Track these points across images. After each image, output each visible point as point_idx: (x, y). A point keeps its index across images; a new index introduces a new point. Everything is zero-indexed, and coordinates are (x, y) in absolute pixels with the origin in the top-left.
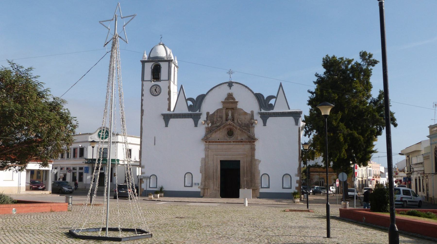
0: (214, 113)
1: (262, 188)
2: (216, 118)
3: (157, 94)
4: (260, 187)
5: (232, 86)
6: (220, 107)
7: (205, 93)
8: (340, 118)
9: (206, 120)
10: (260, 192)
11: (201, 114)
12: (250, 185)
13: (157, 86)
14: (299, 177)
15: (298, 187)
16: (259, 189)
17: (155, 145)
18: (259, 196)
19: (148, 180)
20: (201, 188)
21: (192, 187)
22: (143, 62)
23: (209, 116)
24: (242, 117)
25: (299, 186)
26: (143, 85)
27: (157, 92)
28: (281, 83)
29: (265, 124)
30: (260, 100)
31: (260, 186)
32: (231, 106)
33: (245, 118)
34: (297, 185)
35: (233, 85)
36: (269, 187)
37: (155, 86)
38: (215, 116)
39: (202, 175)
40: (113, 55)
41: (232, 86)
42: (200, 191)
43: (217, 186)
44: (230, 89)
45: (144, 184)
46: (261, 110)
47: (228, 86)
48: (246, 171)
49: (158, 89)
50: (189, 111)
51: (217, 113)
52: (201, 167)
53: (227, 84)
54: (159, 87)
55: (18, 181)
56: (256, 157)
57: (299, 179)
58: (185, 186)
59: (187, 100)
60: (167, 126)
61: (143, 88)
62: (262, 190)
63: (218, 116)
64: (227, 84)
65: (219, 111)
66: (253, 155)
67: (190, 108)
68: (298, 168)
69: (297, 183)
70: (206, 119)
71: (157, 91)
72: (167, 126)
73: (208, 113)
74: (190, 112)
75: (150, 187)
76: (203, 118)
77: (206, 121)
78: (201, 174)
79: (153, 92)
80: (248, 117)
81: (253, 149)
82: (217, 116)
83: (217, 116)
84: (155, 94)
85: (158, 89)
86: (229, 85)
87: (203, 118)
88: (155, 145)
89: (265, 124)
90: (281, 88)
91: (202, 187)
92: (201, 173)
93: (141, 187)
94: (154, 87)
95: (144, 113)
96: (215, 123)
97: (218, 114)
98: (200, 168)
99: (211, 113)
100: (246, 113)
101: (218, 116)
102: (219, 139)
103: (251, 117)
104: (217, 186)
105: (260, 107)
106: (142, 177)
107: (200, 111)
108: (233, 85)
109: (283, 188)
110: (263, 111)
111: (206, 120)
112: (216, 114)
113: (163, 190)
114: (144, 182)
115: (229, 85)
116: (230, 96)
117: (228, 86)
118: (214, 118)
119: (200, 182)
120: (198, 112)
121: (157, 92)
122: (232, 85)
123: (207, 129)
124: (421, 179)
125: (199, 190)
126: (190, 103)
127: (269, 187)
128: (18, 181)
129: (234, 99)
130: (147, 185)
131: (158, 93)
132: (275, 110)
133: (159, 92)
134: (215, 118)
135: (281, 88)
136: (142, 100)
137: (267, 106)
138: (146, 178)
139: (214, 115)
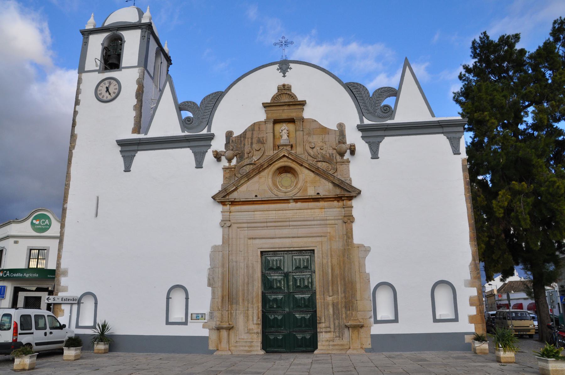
0: (245, 133)
1: (377, 322)
2: (250, 144)
3: (109, 98)
4: (372, 320)
5: (289, 70)
6: (261, 116)
7: (223, 90)
8: (543, 145)
9: (225, 150)
10: (371, 335)
11: (211, 137)
12: (344, 316)
13: (112, 81)
14: (475, 288)
15: (475, 315)
16: (369, 328)
17: (97, 215)
18: (370, 347)
19: (75, 307)
20: (211, 328)
21: (187, 325)
22: (86, 33)
23: (231, 142)
24: (316, 140)
25: (477, 314)
26: (80, 82)
27: (110, 94)
28: (406, 58)
29: (375, 155)
30: (358, 98)
31: (370, 317)
32: (286, 113)
33: (325, 142)
34: (473, 311)
35: (291, 68)
36: (396, 320)
37: (106, 82)
38: (246, 139)
39: (213, 293)
40: (321, 353)
41: (289, 70)
42: (208, 336)
43: (255, 322)
44: (284, 76)
45: (63, 317)
46: (362, 120)
47: (280, 71)
48: (330, 278)
49: (115, 89)
50: (183, 131)
51: (252, 134)
52: (212, 270)
53: (277, 66)
54: (115, 83)
55: (299, 247)
56: (357, 239)
57: (477, 295)
58: (168, 323)
59: (180, 108)
60: (127, 169)
61: (81, 88)
62: (376, 329)
63: (255, 141)
64: (277, 66)
65: (256, 128)
66: (349, 235)
67: (186, 123)
68: (471, 264)
69: (471, 304)
70: (225, 149)
71: (110, 90)
72: (127, 169)
73: (229, 135)
74: (186, 133)
75: (77, 327)
76: (219, 144)
77: (225, 152)
78: (210, 288)
79: (101, 94)
80: (332, 140)
81: (349, 219)
82: (252, 139)
83: (252, 139)
84: (105, 99)
85: (115, 89)
86: (280, 68)
87: (219, 144)
88: (97, 215)
89: (375, 155)
90: (407, 69)
91: (213, 324)
92: (209, 286)
93: (43, 327)
94: (105, 84)
95: (78, 142)
96: (246, 155)
97: (255, 136)
98: (209, 275)
99: (237, 133)
100: (324, 131)
101: (254, 140)
102: (256, 196)
103: (337, 138)
104: (253, 320)
105: (359, 113)
106: (58, 299)
107: (209, 130)
108: (291, 68)
109: (435, 320)
110: (366, 122)
111: (225, 150)
112: (249, 135)
113: (105, 334)
114: (65, 311)
115: (280, 68)
116: (284, 90)
117: (278, 69)
118: (244, 145)
119: (206, 310)
120: (205, 132)
121: (110, 94)
122: (288, 68)
123: (228, 171)
124: (309, 259)
125: (205, 333)
126: (187, 114)
127: (396, 320)
128: (299, 247)
129: (293, 96)
130: (273, 239)
131: (113, 95)
132: (399, 118)
133: (114, 93)
134: (246, 144)
135: (407, 69)
136: (75, 113)
137: (379, 111)
138: (70, 302)
139: (245, 138)
